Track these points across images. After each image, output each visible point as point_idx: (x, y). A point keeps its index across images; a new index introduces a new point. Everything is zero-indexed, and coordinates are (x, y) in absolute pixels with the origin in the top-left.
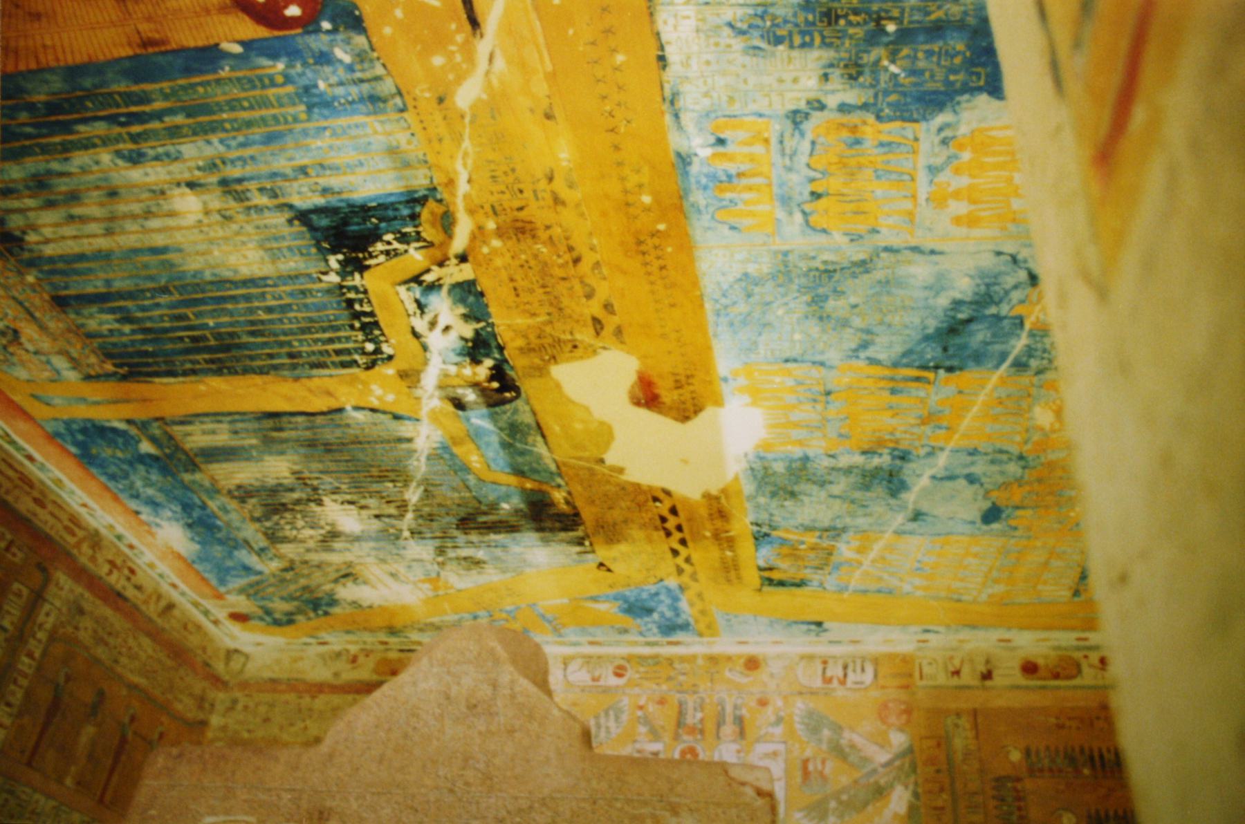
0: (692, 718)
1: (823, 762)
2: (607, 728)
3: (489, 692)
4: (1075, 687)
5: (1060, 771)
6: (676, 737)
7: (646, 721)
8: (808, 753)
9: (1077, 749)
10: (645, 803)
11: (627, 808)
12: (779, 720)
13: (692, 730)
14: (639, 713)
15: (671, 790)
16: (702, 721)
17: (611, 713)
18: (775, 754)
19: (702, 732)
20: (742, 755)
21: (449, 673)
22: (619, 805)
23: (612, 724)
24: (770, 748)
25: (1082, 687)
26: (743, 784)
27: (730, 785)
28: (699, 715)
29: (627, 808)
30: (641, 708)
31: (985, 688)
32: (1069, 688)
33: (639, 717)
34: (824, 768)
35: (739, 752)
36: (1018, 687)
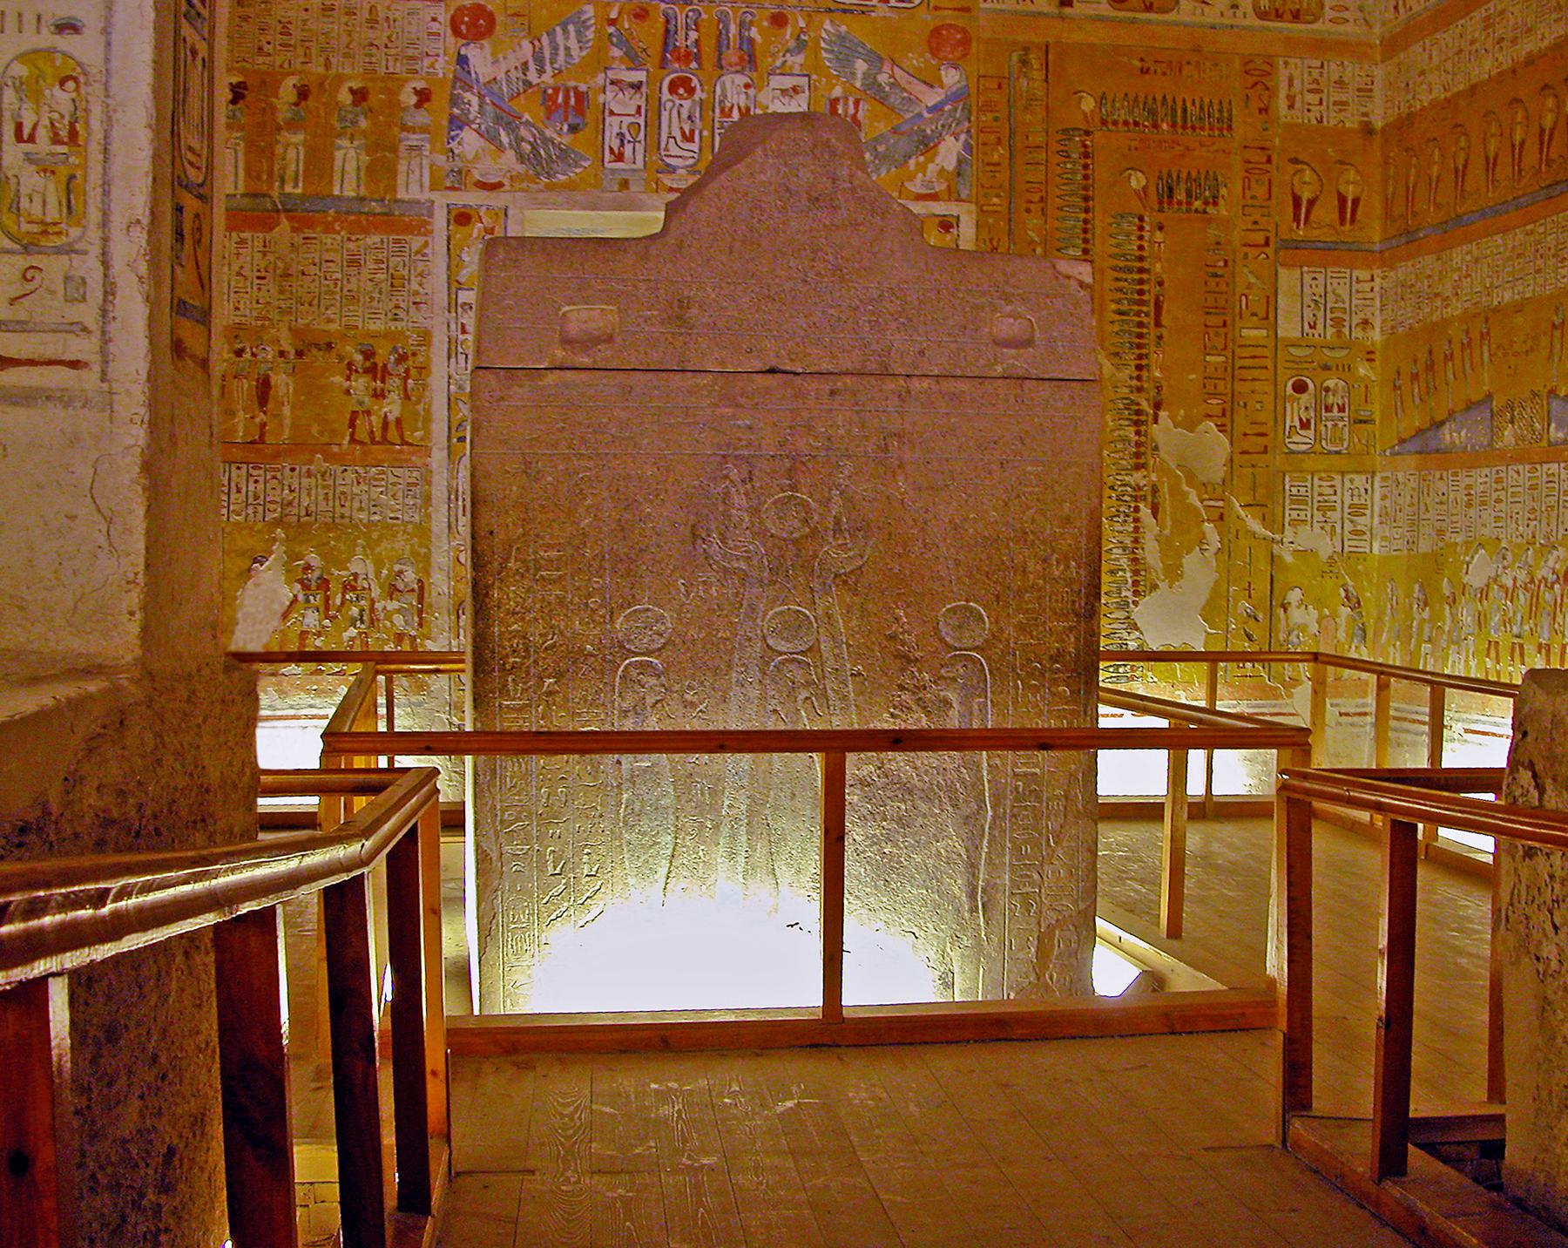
0: (686, 39)
1: (857, 103)
2: (567, 49)
3: (829, 184)
4: (1166, 23)
5: (1136, 124)
6: (663, 64)
7: (624, 41)
8: (837, 92)
9: (1159, 98)
10: (984, 294)
11: (967, 298)
12: (801, 46)
13: (686, 57)
14: (611, 30)
15: (1007, 282)
16: (697, 42)
17: (571, 28)
18: (795, 90)
19: (698, 58)
20: (751, 91)
21: (786, 164)
22: (961, 295)
23: (573, 43)
24: (788, 82)
25: (1177, 24)
26: (1068, 277)
27: (1057, 278)
28: (693, 35)
29: (967, 298)
30: (612, 22)
31: (1062, 18)
32: (1158, 23)
33: (611, 34)
34: (857, 112)
35: (747, 86)
36: (1102, 19)
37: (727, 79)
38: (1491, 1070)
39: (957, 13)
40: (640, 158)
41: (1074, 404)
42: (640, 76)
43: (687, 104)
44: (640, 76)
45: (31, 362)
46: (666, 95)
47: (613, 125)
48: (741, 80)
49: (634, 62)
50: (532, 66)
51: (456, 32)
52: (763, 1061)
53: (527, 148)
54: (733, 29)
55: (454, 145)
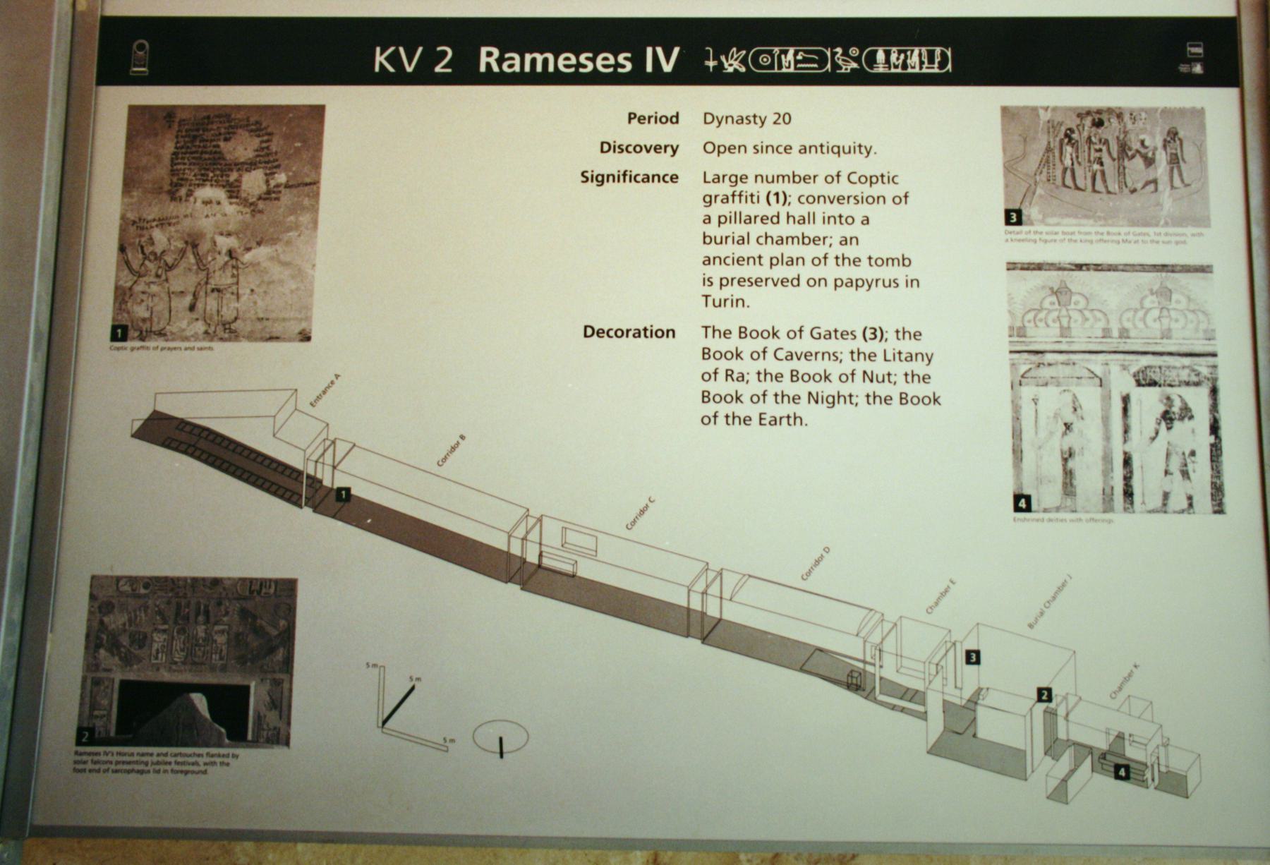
23: (143, 615)
28: (187, 610)
37: (198, 627)
38: (189, 830)
39: (281, 315)
40: (164, 658)
41: (932, 860)
42: (166, 627)
43: (183, 637)
44: (166, 627)
45: (955, 673)
46: (175, 634)
47: (155, 646)
48: (203, 627)
49: (165, 622)
50: (127, 624)
51: (100, 612)
52: (1200, 264)
53: (123, 655)
54: (202, 607)
55: (96, 654)
